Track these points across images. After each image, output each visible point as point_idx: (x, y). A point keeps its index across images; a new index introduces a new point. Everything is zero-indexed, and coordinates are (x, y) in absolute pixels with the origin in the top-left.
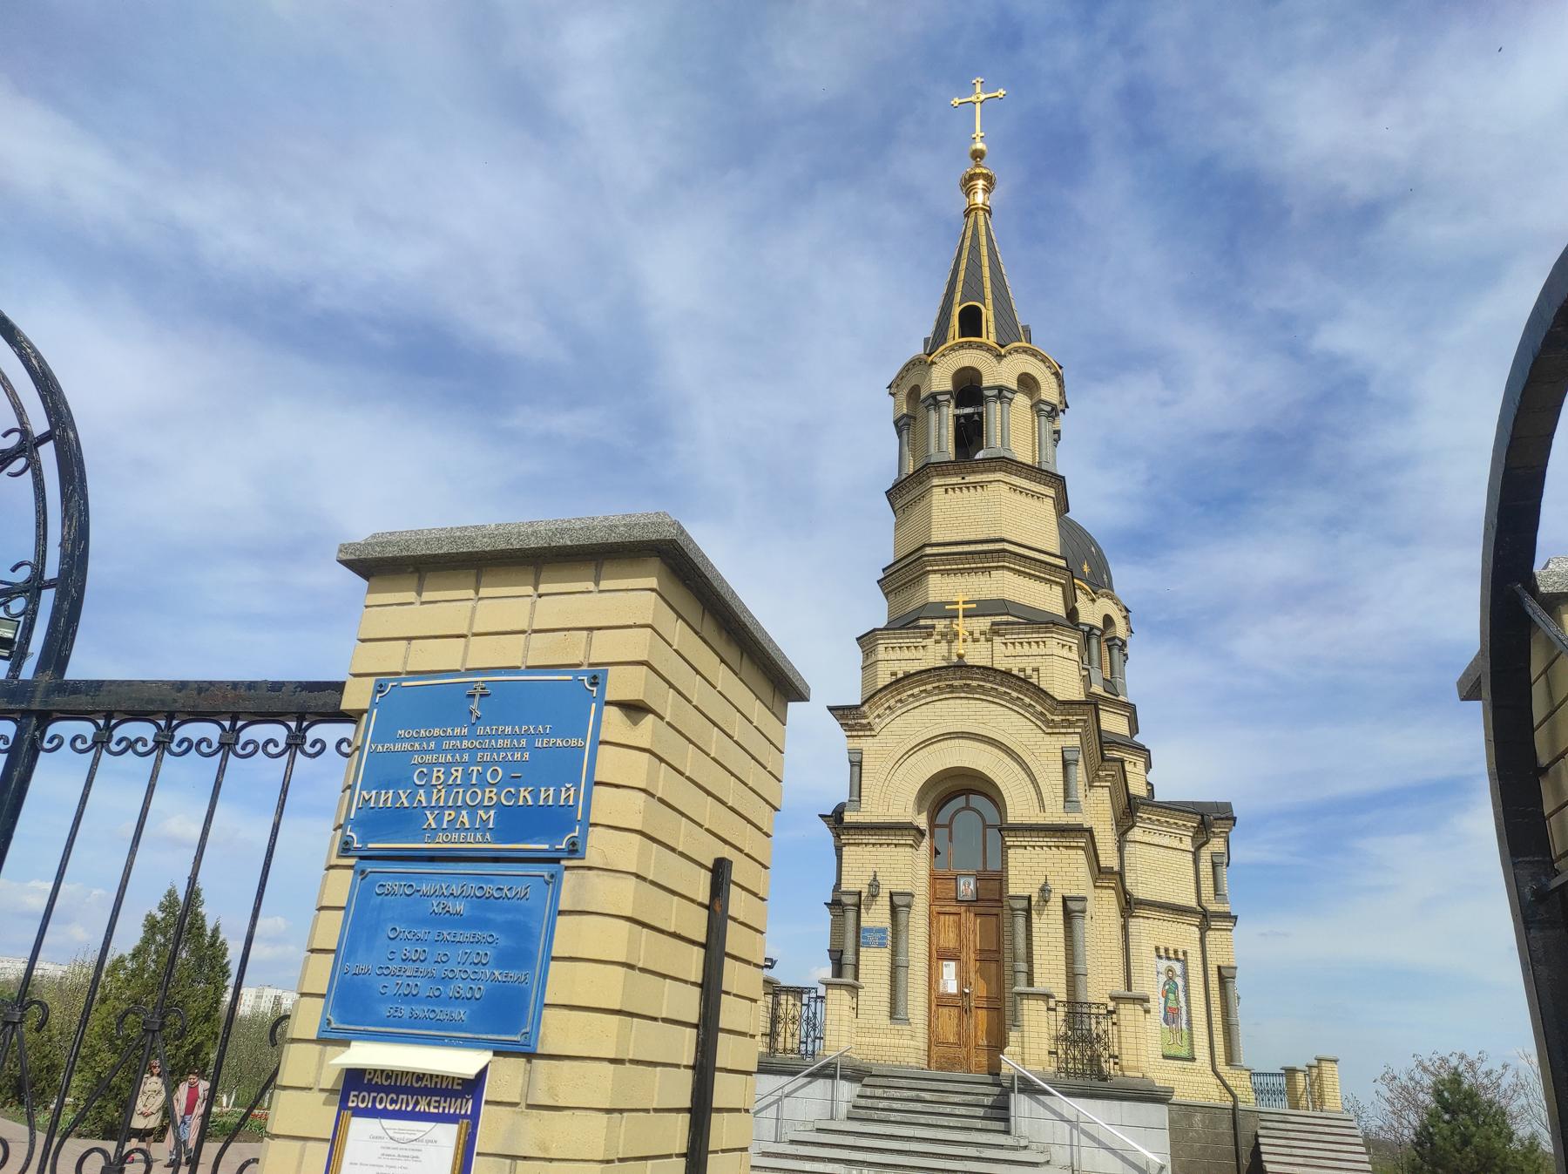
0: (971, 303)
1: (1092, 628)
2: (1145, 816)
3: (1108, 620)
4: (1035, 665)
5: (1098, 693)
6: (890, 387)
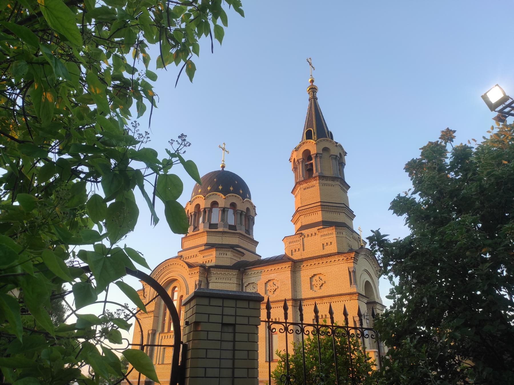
1: (242, 211)
2: (215, 272)
6: (290, 160)
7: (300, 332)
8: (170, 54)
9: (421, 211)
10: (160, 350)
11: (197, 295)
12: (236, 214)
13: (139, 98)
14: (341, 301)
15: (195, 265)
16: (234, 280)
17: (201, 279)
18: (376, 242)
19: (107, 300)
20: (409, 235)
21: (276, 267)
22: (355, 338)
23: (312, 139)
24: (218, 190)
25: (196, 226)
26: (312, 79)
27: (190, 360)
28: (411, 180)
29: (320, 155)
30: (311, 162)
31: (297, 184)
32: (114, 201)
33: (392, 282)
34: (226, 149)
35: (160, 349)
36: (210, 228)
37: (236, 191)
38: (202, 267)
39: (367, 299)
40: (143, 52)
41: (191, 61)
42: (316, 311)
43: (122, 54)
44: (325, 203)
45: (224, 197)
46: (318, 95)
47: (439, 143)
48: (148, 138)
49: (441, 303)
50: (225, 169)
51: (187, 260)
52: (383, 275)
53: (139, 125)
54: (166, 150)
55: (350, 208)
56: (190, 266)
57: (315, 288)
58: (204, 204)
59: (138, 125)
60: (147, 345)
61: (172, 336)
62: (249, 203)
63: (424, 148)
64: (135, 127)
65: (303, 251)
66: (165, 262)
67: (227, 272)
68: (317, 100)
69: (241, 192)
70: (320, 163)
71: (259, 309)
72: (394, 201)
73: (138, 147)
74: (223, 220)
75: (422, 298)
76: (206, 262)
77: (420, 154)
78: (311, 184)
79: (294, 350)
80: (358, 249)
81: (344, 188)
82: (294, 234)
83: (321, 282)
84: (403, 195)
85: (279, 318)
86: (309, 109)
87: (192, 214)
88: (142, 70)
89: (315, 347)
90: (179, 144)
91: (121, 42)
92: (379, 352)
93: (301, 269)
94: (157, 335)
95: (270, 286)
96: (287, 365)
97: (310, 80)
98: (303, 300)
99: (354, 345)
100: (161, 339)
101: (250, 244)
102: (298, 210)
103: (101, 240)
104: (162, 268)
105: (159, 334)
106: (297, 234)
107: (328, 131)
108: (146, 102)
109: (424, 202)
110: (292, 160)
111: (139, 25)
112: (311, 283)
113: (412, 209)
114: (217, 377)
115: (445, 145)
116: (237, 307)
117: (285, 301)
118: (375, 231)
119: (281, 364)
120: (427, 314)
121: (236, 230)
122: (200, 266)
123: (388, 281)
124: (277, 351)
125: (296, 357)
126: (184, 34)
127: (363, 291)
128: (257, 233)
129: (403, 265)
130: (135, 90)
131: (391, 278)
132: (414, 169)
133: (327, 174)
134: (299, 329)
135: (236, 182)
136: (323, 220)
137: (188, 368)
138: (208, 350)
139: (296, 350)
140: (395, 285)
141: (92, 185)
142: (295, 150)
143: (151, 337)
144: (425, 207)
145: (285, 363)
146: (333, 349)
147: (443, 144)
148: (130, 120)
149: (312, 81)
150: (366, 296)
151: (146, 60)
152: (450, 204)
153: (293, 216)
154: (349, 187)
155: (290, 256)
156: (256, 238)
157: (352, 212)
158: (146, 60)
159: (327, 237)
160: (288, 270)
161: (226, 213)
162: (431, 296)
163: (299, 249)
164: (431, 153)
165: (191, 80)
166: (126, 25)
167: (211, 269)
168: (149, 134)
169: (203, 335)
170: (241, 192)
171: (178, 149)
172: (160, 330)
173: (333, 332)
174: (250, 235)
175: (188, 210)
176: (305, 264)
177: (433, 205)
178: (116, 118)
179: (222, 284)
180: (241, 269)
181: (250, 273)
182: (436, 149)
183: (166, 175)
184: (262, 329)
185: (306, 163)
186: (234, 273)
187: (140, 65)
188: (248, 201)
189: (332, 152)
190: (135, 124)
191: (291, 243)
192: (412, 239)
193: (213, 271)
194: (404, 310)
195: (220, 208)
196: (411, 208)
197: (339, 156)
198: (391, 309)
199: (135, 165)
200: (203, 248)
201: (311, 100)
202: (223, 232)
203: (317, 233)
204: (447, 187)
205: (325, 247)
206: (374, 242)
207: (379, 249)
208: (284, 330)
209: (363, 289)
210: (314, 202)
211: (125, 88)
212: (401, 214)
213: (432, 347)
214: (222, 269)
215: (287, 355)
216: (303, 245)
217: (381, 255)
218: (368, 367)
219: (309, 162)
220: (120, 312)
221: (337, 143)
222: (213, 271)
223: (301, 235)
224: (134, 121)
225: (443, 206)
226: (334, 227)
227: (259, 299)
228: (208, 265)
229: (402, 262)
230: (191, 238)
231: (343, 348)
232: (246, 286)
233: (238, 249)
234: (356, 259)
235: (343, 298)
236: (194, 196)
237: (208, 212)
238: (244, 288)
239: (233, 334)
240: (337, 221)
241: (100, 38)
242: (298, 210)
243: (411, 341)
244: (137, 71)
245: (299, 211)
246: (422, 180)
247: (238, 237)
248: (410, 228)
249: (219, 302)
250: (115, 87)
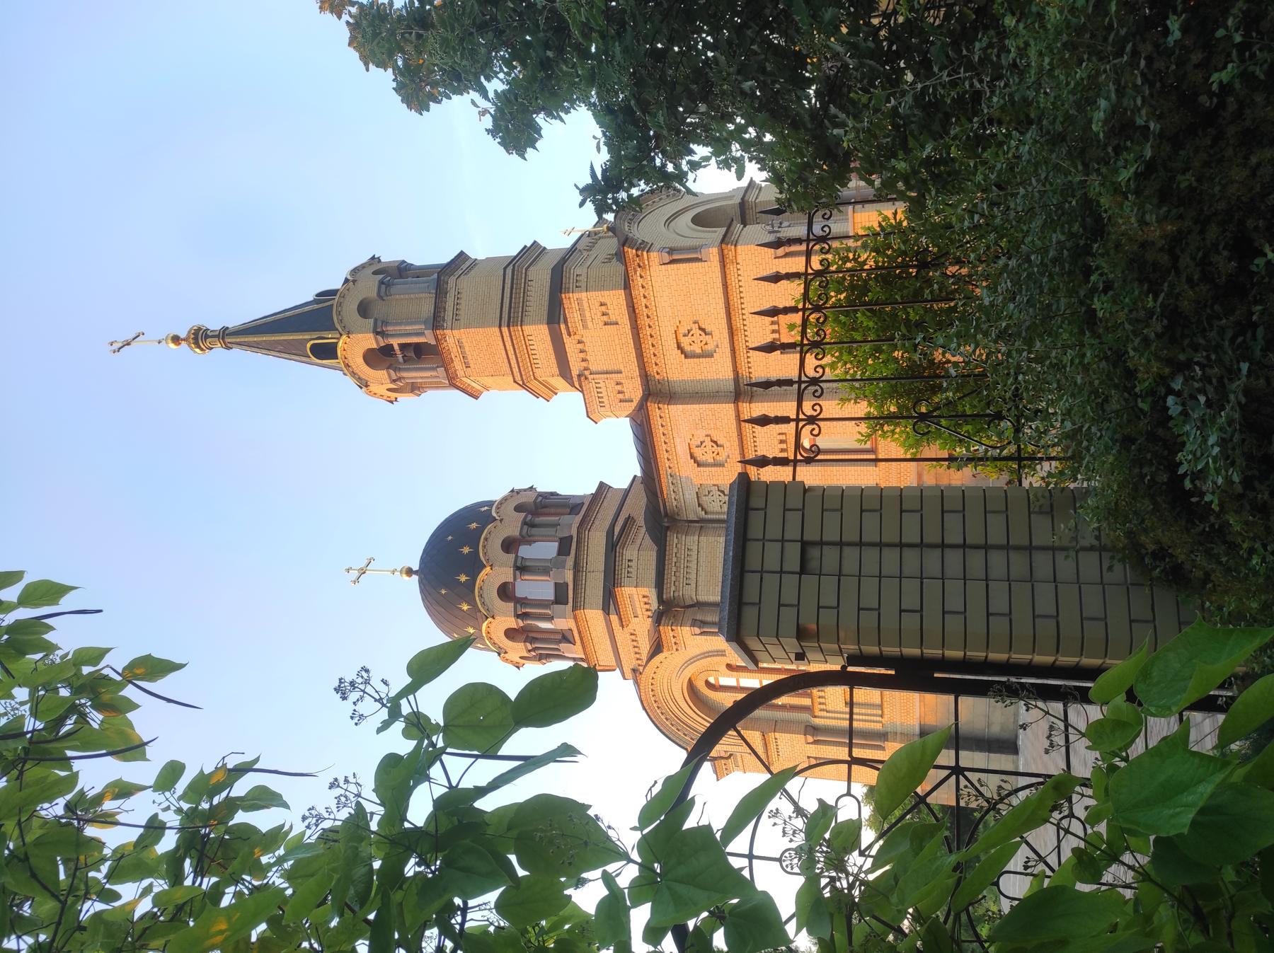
0: (309, 346)
1: (525, 523)
2: (673, 588)
4: (597, 304)
5: (573, 560)
6: (392, 402)
7: (817, 387)
8: (106, 726)
9: (531, 79)
10: (862, 714)
11: (736, 636)
12: (532, 538)
13: (233, 805)
14: (740, 286)
15: (657, 635)
16: (691, 540)
17: (690, 622)
18: (610, 196)
19: (747, 853)
20: (590, 113)
21: (659, 439)
22: (830, 257)
23: (337, 343)
24: (471, 585)
25: (559, 637)
26: (169, 341)
27: (883, 649)
28: (450, 98)
29: (379, 323)
30: (396, 347)
32: (513, 858)
33: (703, 164)
34: (363, 565)
35: (859, 714)
36: (566, 603)
37: (473, 539)
38: (661, 619)
39: (735, 221)
40: (99, 799)
41: (124, 669)
42: (769, 348)
43: (104, 860)
44: (503, 316)
45: (488, 568)
46: (215, 325)
47: (351, 21)
48: (346, 781)
49: (755, 47)
51: (644, 657)
52: (687, 184)
53: (313, 808)
54: (379, 731)
55: (515, 254)
56: (657, 648)
57: (710, 347)
58: (506, 619)
59: (313, 812)
60: (851, 746)
62: (504, 506)
63: (366, 60)
64: (320, 818)
65: (621, 372)
66: (648, 711)
67: (671, 559)
68: (227, 328)
69: (474, 525)
70: (400, 324)
71: (768, 486)
72: (503, 144)
73: (375, 810)
74: (545, 571)
75: (743, 93)
76: (647, 610)
77: (382, 70)
78: (455, 350)
79: (856, 402)
80: (615, 240)
82: (581, 394)
83: (696, 331)
84: (488, 122)
85: (780, 434)
86: (253, 349)
87: (530, 648)
88: (154, 802)
89: (850, 352)
90: (362, 697)
91: (72, 865)
92: (864, 202)
93: (664, 380)
94: (817, 721)
95: (706, 455)
96: (891, 418)
97: (172, 346)
98: (738, 376)
99: (846, 260)
100: (827, 711)
101: (605, 503)
102: (521, 383)
103: (622, 890)
104: (663, 717)
105: (815, 717)
106: (581, 386)
107: (314, 302)
108: (241, 788)
109: (506, 70)
110: (393, 395)
111: (19, 820)
112: (699, 356)
113: (525, 102)
114: (922, 583)
115: (356, 7)
116: (762, 537)
117: (739, 421)
118: (581, 198)
119: (888, 431)
120: (780, 83)
121: (572, 536)
122: (659, 626)
123: (700, 172)
124: (859, 441)
125: (879, 399)
126: (47, 691)
127: (715, 232)
128: (582, 487)
129: (665, 132)
130: (209, 819)
131: (695, 166)
132: (421, 89)
133: (427, 308)
134: (812, 388)
135: (450, 538)
136: (545, 321)
137: (901, 651)
138: (861, 606)
139: (857, 397)
140: (710, 155)
141: (472, 919)
142: (364, 389)
143: (821, 736)
144: (518, 71)
145: (887, 423)
146: (856, 311)
147: (354, 10)
148: (291, 827)
149: (176, 339)
150: (727, 224)
151: (123, 790)
152: (512, 6)
153: (537, 395)
154: (462, 253)
155: (634, 404)
156: (592, 489)
157: (525, 250)
158: (123, 790)
159: (588, 314)
160: (667, 411)
161: (528, 564)
162: (739, 72)
163: (617, 384)
164: (379, 43)
165: (179, 667)
166: (22, 857)
167: (664, 597)
168: (336, 780)
169: (828, 618)
170: (474, 525)
171: (376, 700)
172: (804, 716)
173: (817, 309)
174: (583, 504)
175: (521, 658)
176: (652, 370)
177: (513, 48)
178: (287, 865)
179: (700, 569)
180: (666, 525)
181: (675, 503)
182: (369, 30)
183: (447, 729)
184: (810, 476)
185: (401, 360)
186: (676, 541)
187: (139, 809)
188: (498, 508)
189: (372, 293)
190: (310, 820)
191: (603, 402)
192: (601, 106)
194: (768, 138)
195: (515, 579)
196: (522, 104)
198: (765, 170)
199: (419, 810)
200: (614, 618)
201: (229, 345)
202: (577, 569)
203: (577, 337)
204: (468, 11)
205: (613, 319)
206: (610, 201)
207: (627, 190)
208: (815, 426)
209: (712, 232)
210: (501, 344)
211: (204, 844)
212: (538, 130)
213: (855, 78)
214: (664, 570)
215: (868, 418)
216: (607, 373)
217: (640, 185)
218: (897, 229)
219: (398, 352)
220: (789, 830)
221: (347, 281)
223: (582, 378)
224: (303, 821)
225: (515, 24)
226: (563, 295)
227: (744, 485)
228: (654, 605)
229: (657, 136)
230: (590, 648)
231: (852, 287)
232: (706, 513)
233: (616, 533)
234: (641, 244)
235: (733, 279)
236: (485, 644)
237: (525, 607)
238: (709, 516)
239: (824, 547)
240: (548, 289)
241: (59, 923)
242: (521, 383)
243: (842, 125)
244: (156, 815)
245: (522, 380)
246: (450, 71)
247: (587, 532)
248: (572, 110)
249: (752, 581)
250: (200, 871)
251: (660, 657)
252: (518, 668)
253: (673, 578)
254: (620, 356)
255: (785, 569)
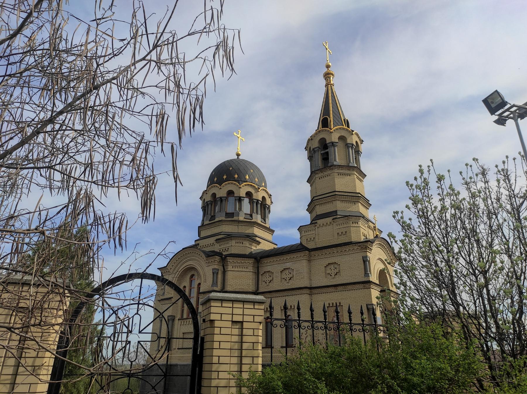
1: (258, 200)
2: (231, 261)
3: (264, 198)
6: (305, 148)
16: (251, 269)
31: (312, 172)
39: (381, 288)
50: (240, 157)
61: (191, 322)
80: (372, 238)
81: (361, 178)
110: (308, 149)
179: (239, 272)
181: (266, 262)
186: (250, 262)
188: (264, 190)
193: (230, 259)
197: (355, 144)
222: (230, 259)
232: (262, 275)
236: (210, 185)
251: (204, 256)
252: (200, 198)
253: (235, 261)
254: (324, 239)
255: (234, 315)
